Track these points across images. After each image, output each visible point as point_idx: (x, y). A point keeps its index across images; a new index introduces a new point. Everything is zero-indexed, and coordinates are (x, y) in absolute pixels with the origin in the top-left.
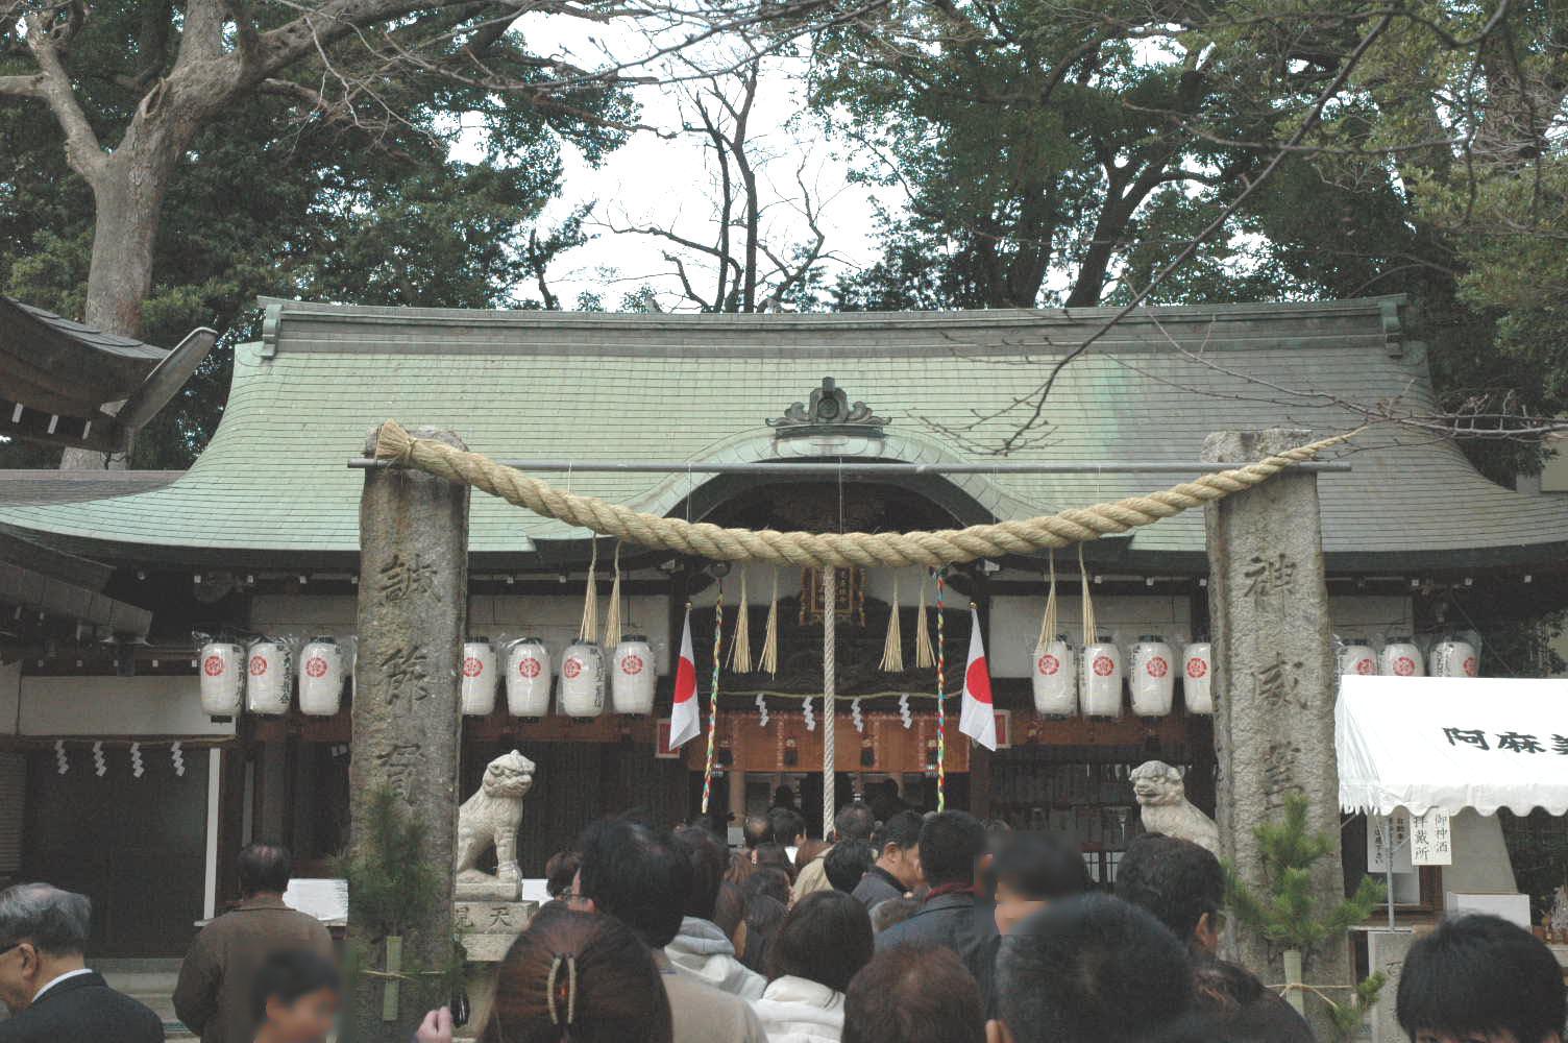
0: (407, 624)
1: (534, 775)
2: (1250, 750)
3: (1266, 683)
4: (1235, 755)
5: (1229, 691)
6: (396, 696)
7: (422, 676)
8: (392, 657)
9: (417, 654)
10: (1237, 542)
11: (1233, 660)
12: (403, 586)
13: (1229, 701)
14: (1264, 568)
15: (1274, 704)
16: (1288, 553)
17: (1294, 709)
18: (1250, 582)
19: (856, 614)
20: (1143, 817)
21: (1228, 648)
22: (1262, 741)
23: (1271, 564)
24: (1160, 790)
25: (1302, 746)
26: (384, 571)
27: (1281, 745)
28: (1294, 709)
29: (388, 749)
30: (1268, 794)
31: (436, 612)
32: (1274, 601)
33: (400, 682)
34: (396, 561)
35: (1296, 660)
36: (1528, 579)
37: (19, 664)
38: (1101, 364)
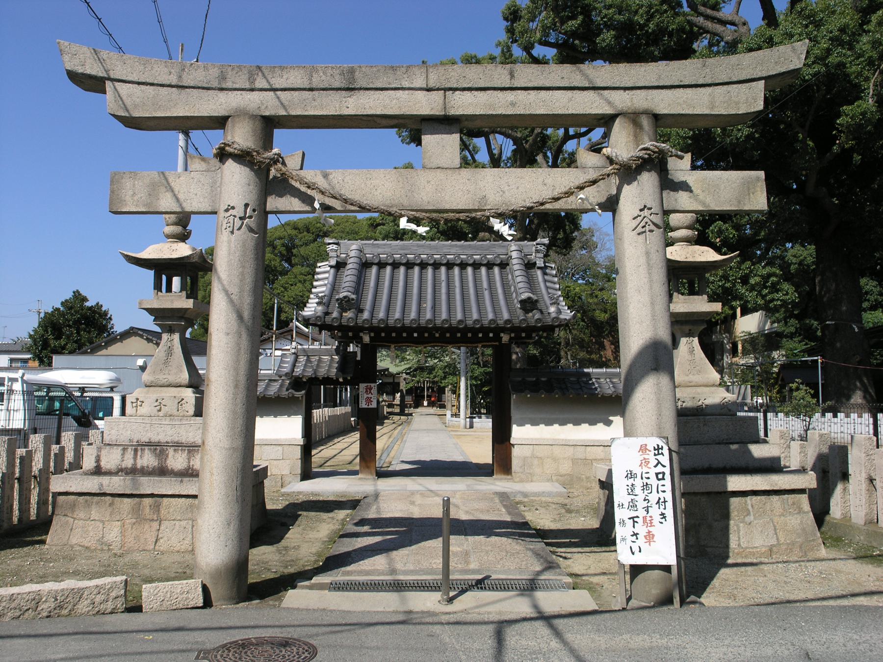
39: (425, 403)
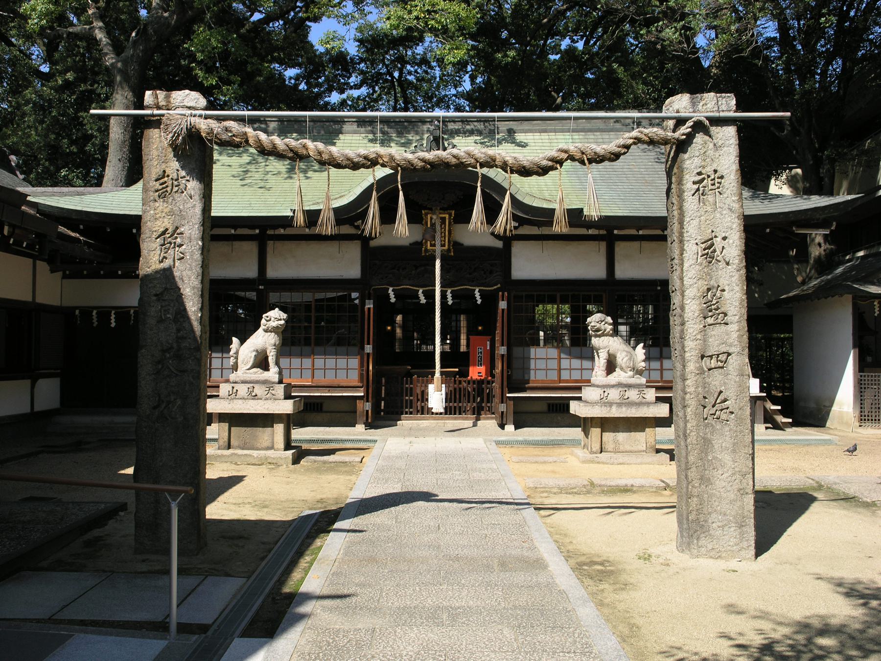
0: (171, 213)
1: (287, 321)
2: (695, 290)
3: (705, 249)
4: (686, 294)
5: (682, 254)
6: (165, 258)
7: (180, 246)
8: (164, 233)
9: (178, 231)
10: (688, 162)
11: (685, 235)
12: (169, 189)
13: (682, 260)
14: (704, 179)
15: (710, 262)
16: (718, 169)
17: (722, 265)
18: (696, 186)
19: (449, 250)
20: (593, 342)
21: (682, 227)
22: (703, 285)
23: (709, 176)
24: (603, 328)
25: (726, 288)
26: (156, 180)
27: (713, 287)
28: (722, 265)
29: (161, 290)
30: (705, 318)
31: (189, 205)
32: (710, 198)
33: (169, 249)
34: (164, 174)
35: (724, 235)
36: (768, 230)
37: (60, 274)
38: (562, 137)
39: (436, 397)
